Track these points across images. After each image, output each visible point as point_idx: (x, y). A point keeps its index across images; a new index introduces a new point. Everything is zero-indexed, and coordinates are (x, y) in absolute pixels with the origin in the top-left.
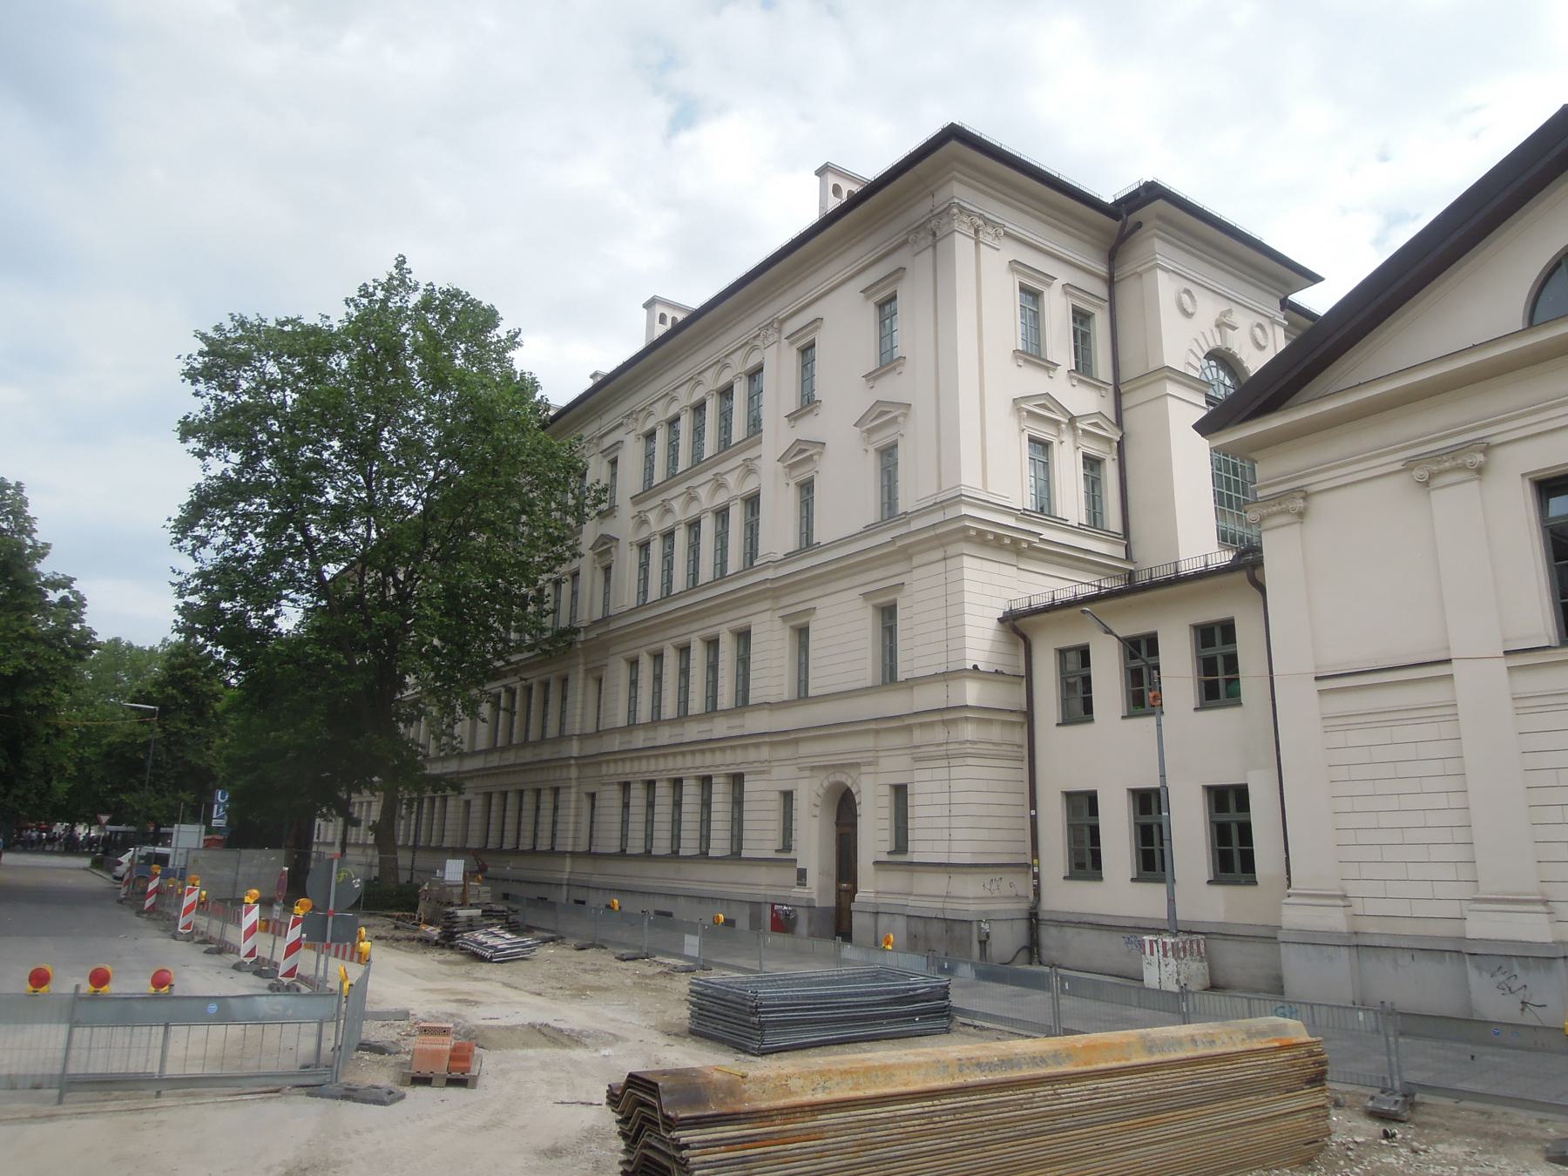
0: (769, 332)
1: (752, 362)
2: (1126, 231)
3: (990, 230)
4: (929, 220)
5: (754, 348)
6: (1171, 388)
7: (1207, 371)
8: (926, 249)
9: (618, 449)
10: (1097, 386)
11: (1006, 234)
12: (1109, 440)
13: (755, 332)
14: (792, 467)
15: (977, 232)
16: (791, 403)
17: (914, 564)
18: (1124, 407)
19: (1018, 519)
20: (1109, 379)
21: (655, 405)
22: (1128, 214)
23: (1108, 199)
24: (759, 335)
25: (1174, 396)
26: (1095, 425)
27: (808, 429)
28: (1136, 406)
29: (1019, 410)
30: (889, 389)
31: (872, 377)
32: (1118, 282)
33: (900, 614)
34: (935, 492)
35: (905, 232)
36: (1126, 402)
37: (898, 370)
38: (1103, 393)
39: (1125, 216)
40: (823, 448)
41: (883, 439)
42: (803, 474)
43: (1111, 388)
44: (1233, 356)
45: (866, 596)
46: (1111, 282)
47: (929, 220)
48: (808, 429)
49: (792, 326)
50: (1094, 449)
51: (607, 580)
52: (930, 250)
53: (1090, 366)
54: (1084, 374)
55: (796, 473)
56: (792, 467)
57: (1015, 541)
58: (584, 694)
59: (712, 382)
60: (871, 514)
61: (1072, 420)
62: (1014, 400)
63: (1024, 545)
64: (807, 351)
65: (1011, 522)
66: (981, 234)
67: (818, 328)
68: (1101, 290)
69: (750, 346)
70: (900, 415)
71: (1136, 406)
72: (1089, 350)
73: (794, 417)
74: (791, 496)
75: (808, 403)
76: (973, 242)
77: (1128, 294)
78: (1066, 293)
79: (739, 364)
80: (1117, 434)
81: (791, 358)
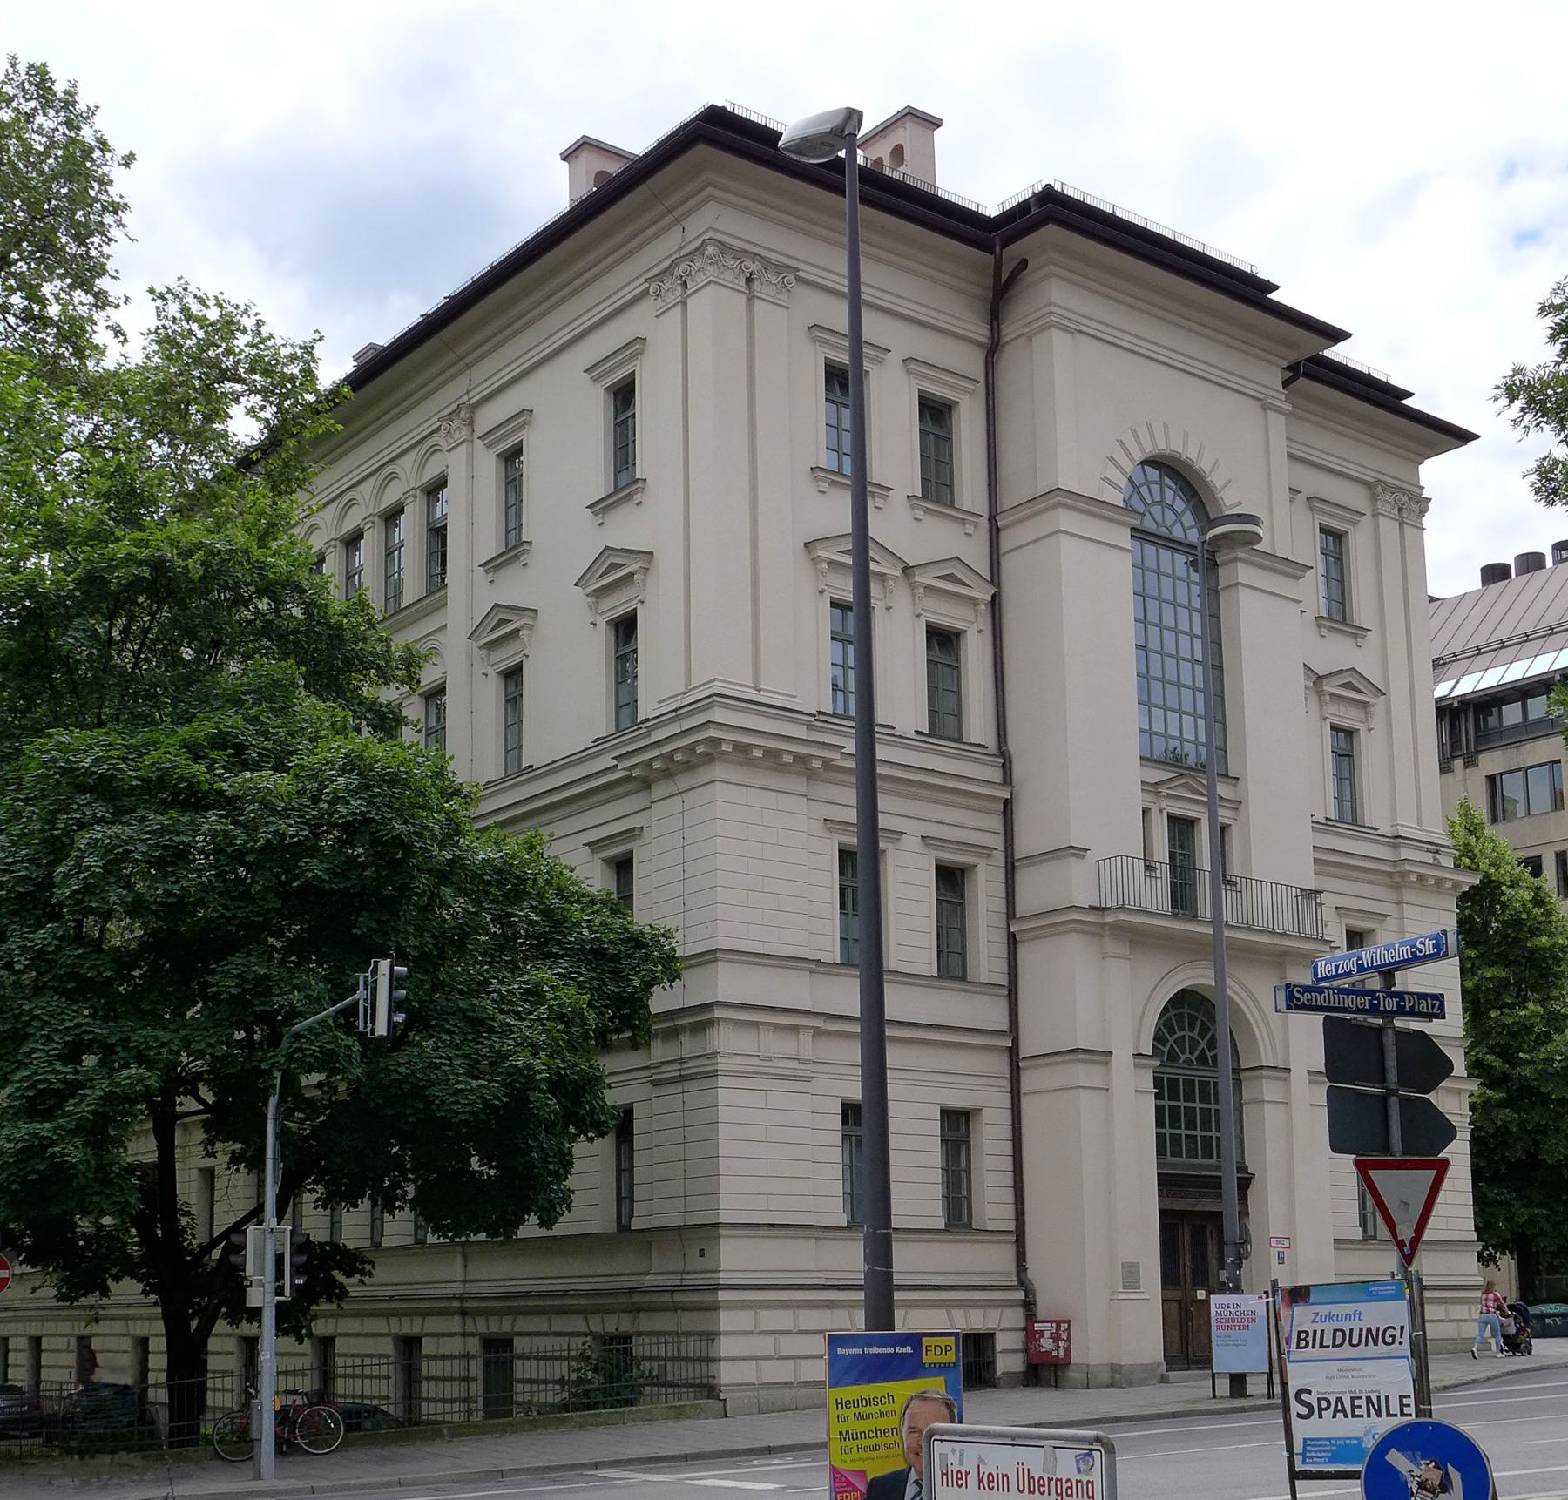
0: (454, 425)
1: (430, 474)
2: (1004, 278)
3: (772, 278)
4: (675, 264)
5: (435, 450)
6: (1066, 520)
7: (1144, 490)
8: (674, 306)
9: (522, 426)
10: (963, 518)
11: (802, 281)
12: (974, 602)
13: (433, 424)
14: (600, 593)
15: (749, 280)
16: (490, 546)
17: (654, 797)
18: (1003, 549)
19: (810, 727)
20: (982, 507)
21: (402, 461)
22: (1004, 246)
23: (992, 210)
24: (439, 429)
25: (1067, 533)
26: (950, 578)
27: (514, 589)
28: (1012, 550)
29: (815, 560)
30: (627, 529)
31: (602, 507)
32: (1008, 343)
33: (638, 870)
34: (683, 690)
35: (643, 279)
36: (1006, 543)
37: (637, 498)
38: (969, 529)
39: (998, 249)
40: (534, 619)
41: (617, 605)
42: (506, 657)
43: (984, 522)
44: (1186, 465)
45: (594, 846)
46: (993, 350)
47: (675, 264)
48: (514, 589)
49: (490, 416)
50: (949, 616)
51: (513, 701)
52: (679, 307)
53: (951, 486)
54: (938, 501)
55: (605, 604)
56: (600, 593)
57: (801, 759)
58: (1466, 721)
59: (368, 502)
60: (602, 724)
61: (907, 569)
62: (806, 544)
63: (817, 764)
64: (512, 456)
65: (800, 732)
66: (756, 285)
67: (640, 352)
68: (972, 362)
69: (424, 445)
70: (637, 572)
71: (1012, 550)
72: (950, 463)
73: (494, 566)
74: (491, 691)
75: (513, 550)
76: (744, 298)
77: (1012, 363)
78: (909, 372)
79: (409, 476)
80: (987, 593)
81: (488, 466)
